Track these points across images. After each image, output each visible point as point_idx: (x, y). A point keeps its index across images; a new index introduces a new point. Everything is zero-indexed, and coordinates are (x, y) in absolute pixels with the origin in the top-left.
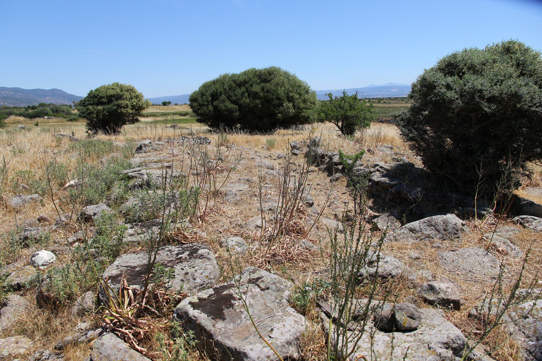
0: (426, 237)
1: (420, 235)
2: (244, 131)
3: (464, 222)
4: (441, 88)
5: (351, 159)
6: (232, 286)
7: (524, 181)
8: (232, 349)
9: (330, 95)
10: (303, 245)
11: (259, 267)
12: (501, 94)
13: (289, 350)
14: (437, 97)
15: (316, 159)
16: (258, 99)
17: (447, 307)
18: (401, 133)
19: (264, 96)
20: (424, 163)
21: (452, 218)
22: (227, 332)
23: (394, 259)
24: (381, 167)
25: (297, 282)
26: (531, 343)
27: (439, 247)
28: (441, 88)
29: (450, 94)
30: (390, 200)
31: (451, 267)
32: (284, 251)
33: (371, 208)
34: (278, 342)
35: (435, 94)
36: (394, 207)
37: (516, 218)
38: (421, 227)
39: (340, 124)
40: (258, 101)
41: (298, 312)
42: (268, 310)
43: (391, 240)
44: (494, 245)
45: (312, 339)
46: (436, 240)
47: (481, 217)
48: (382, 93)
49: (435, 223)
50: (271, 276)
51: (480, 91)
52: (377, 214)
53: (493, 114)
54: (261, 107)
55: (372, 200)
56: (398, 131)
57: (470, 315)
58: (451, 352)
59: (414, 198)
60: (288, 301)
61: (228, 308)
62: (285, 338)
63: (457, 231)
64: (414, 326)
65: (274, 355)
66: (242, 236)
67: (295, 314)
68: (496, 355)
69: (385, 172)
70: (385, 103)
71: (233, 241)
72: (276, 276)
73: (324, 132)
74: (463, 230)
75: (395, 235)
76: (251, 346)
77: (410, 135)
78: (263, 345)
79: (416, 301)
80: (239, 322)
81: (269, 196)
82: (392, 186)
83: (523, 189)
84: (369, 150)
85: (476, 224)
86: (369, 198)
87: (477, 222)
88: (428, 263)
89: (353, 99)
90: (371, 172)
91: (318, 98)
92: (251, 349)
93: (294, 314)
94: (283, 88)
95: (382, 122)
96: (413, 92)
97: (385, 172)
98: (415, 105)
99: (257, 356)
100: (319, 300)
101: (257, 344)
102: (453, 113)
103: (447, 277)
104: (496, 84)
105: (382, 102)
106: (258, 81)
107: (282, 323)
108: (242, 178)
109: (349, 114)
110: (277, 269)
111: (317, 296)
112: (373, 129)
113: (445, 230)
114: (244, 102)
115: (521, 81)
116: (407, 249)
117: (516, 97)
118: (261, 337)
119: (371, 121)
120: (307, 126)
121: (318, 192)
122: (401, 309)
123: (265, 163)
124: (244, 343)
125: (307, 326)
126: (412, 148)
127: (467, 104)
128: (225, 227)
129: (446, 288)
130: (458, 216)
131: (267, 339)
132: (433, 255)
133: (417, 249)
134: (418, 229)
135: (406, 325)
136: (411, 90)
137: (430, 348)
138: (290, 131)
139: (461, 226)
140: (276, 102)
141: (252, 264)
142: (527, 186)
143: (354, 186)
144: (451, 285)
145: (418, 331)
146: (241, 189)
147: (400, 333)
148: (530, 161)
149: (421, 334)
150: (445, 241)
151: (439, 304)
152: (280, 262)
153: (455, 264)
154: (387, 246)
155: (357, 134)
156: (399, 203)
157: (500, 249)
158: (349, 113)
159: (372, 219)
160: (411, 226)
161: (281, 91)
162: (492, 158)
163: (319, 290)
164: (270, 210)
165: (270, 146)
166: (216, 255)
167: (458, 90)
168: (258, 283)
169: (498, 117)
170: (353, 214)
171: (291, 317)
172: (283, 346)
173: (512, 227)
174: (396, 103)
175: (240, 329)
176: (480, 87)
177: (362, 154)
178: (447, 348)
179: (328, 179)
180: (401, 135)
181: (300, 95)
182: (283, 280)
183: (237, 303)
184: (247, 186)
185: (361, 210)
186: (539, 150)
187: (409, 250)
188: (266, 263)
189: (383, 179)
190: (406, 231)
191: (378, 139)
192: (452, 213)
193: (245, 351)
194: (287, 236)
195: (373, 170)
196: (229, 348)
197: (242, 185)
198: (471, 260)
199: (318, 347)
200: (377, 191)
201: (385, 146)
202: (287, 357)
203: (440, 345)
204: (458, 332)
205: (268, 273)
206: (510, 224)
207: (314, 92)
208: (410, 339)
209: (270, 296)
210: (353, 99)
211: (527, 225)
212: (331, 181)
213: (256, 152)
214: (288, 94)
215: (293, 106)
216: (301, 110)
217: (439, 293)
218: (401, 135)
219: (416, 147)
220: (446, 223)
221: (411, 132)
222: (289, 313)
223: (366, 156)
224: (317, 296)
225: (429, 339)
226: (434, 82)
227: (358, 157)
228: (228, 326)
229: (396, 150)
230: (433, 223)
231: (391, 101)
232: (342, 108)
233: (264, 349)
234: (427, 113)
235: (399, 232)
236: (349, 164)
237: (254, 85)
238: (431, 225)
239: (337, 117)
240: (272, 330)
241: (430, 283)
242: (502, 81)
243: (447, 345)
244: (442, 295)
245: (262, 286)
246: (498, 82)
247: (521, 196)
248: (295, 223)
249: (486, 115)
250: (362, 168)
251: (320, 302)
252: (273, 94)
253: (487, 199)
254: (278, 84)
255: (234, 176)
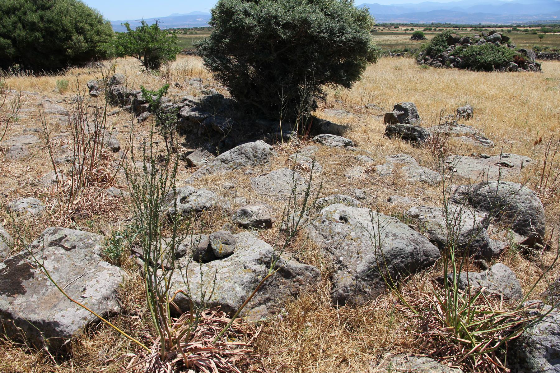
0: (238, 166)
1: (232, 164)
2: (25, 72)
3: (272, 147)
4: (239, 14)
5: (156, 95)
6: (27, 254)
7: (319, 103)
8: (39, 323)
9: (127, 25)
10: (111, 193)
11: (62, 226)
12: (294, 20)
13: (108, 305)
14: (236, 23)
15: (117, 99)
16: (38, 31)
17: (260, 227)
18: (205, 63)
19: (45, 27)
20: (231, 93)
21: (261, 144)
22: (30, 305)
23: (206, 192)
24: (190, 101)
25: (107, 233)
26: (328, 242)
27: (251, 174)
28: (239, 14)
29: (249, 21)
30: (202, 134)
31: (263, 190)
32: (89, 203)
33: (184, 145)
34: (93, 300)
35: (234, 20)
36: (207, 141)
37: (316, 137)
38: (233, 157)
39: (143, 58)
40: (38, 34)
41: (112, 264)
42: (78, 269)
43: (204, 174)
44: (299, 164)
45: (130, 289)
46: (248, 167)
47: (287, 140)
48: (188, 22)
49: (245, 151)
50: (76, 233)
51: (276, 17)
52: (190, 150)
53: (289, 41)
54: (44, 42)
55: (184, 137)
56: (202, 61)
57: (281, 231)
58: (265, 266)
59: (224, 130)
60: (100, 256)
61: (26, 279)
62: (100, 294)
63: (266, 155)
64: (230, 251)
65: (91, 314)
66: (35, 195)
67: (110, 266)
68: (303, 259)
69: (195, 106)
70: (191, 33)
71: (23, 203)
72: (82, 232)
73: (128, 68)
74: (272, 154)
75: (208, 168)
76: (62, 312)
77: (214, 65)
78: (75, 309)
79: (232, 227)
80: (44, 290)
81: (66, 146)
82: (202, 120)
83: (322, 110)
84: (177, 85)
85: (283, 147)
86: (181, 135)
87: (284, 145)
88: (242, 190)
89: (153, 29)
90: (180, 108)
91: (114, 30)
92: (62, 316)
93: (108, 267)
94: (69, 18)
95: (190, 54)
96: (214, 19)
97: (195, 106)
98: (215, 33)
99: (71, 321)
100: (134, 247)
101: (69, 309)
102: (253, 40)
103: (260, 201)
104: (289, 11)
105: (188, 33)
106: (34, 8)
107: (95, 280)
108: (28, 129)
109: (151, 47)
110: (83, 224)
111: (131, 244)
112: (179, 63)
113: (255, 157)
114: (19, 36)
115: (309, 8)
116: (221, 180)
117: (306, 23)
118: (72, 301)
119: (176, 53)
120: (106, 63)
121: (126, 135)
122: (215, 238)
123: (57, 109)
124: (53, 312)
125: (123, 276)
126: (217, 78)
127: (264, 30)
128: (13, 189)
129: (259, 210)
130: (267, 142)
131: (79, 300)
132: (246, 182)
133: (231, 178)
134: (229, 159)
135: (222, 252)
136: (211, 17)
137: (245, 268)
138: (86, 70)
139: (269, 151)
140: (62, 34)
141: (53, 224)
142: (325, 108)
143: (163, 123)
144: (262, 206)
145: (234, 255)
146: (28, 141)
147: (218, 261)
148: (324, 84)
149: (237, 257)
150: (256, 167)
151: (253, 226)
152: (87, 216)
153: (266, 187)
154: (201, 180)
155: (163, 68)
156: (212, 137)
157: (304, 167)
158: (151, 46)
159: (186, 156)
160: (223, 157)
161: (66, 21)
162: (291, 83)
163: (132, 237)
164: (67, 161)
165: (63, 88)
166: (4, 223)
167: (255, 16)
168: (61, 244)
169: (293, 43)
170: (167, 154)
171: (106, 271)
172: (100, 303)
173: (313, 146)
174: (203, 34)
175: (47, 298)
176: (274, 13)
177: (167, 88)
178: (260, 264)
179: (135, 121)
180: (204, 65)
181: (91, 25)
182: (91, 234)
183: (37, 271)
184: (36, 138)
185: (173, 148)
186: (328, 73)
187: (223, 181)
188: (69, 220)
189: (193, 113)
190: (219, 163)
191: (186, 72)
192: (259, 139)
193: (55, 320)
194: (91, 187)
195: (182, 105)
196: (35, 323)
197: (29, 137)
198: (280, 181)
199: (140, 294)
200: (189, 126)
201: (191, 79)
202: (106, 312)
203: (254, 263)
204: (269, 247)
205: (74, 230)
206: (311, 144)
207: (108, 22)
208: (227, 263)
209: (78, 255)
210: (153, 29)
211: (324, 142)
212: (138, 122)
213: (44, 97)
214: (76, 24)
215: (85, 39)
216: (96, 43)
217: (252, 216)
218: (204, 65)
219: (222, 77)
220: (255, 149)
221: (215, 62)
222: (102, 267)
223: (173, 91)
224: (131, 244)
225: (244, 260)
226: (231, 7)
227: (162, 93)
228: (31, 299)
229: (206, 83)
230: (243, 151)
231: (198, 32)
232: (142, 40)
233: (78, 311)
234: (228, 40)
235: (212, 164)
236: (154, 101)
237: (28, 13)
238: (242, 153)
239: (138, 50)
240: (85, 289)
241: (243, 208)
242: (294, 8)
243: (260, 261)
244: (255, 218)
245: (67, 245)
246: (290, 8)
247: (321, 118)
248: (98, 171)
249: (282, 42)
250: (171, 104)
251: (135, 248)
252: (56, 25)
253: (290, 121)
254: (61, 12)
255: (17, 128)
